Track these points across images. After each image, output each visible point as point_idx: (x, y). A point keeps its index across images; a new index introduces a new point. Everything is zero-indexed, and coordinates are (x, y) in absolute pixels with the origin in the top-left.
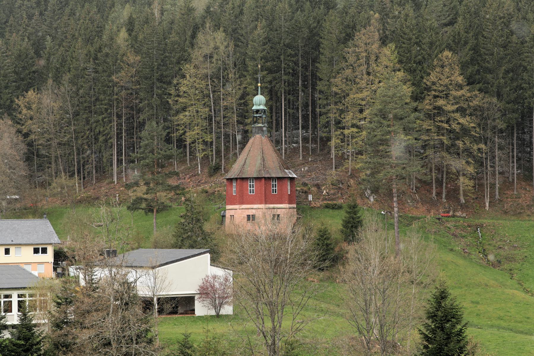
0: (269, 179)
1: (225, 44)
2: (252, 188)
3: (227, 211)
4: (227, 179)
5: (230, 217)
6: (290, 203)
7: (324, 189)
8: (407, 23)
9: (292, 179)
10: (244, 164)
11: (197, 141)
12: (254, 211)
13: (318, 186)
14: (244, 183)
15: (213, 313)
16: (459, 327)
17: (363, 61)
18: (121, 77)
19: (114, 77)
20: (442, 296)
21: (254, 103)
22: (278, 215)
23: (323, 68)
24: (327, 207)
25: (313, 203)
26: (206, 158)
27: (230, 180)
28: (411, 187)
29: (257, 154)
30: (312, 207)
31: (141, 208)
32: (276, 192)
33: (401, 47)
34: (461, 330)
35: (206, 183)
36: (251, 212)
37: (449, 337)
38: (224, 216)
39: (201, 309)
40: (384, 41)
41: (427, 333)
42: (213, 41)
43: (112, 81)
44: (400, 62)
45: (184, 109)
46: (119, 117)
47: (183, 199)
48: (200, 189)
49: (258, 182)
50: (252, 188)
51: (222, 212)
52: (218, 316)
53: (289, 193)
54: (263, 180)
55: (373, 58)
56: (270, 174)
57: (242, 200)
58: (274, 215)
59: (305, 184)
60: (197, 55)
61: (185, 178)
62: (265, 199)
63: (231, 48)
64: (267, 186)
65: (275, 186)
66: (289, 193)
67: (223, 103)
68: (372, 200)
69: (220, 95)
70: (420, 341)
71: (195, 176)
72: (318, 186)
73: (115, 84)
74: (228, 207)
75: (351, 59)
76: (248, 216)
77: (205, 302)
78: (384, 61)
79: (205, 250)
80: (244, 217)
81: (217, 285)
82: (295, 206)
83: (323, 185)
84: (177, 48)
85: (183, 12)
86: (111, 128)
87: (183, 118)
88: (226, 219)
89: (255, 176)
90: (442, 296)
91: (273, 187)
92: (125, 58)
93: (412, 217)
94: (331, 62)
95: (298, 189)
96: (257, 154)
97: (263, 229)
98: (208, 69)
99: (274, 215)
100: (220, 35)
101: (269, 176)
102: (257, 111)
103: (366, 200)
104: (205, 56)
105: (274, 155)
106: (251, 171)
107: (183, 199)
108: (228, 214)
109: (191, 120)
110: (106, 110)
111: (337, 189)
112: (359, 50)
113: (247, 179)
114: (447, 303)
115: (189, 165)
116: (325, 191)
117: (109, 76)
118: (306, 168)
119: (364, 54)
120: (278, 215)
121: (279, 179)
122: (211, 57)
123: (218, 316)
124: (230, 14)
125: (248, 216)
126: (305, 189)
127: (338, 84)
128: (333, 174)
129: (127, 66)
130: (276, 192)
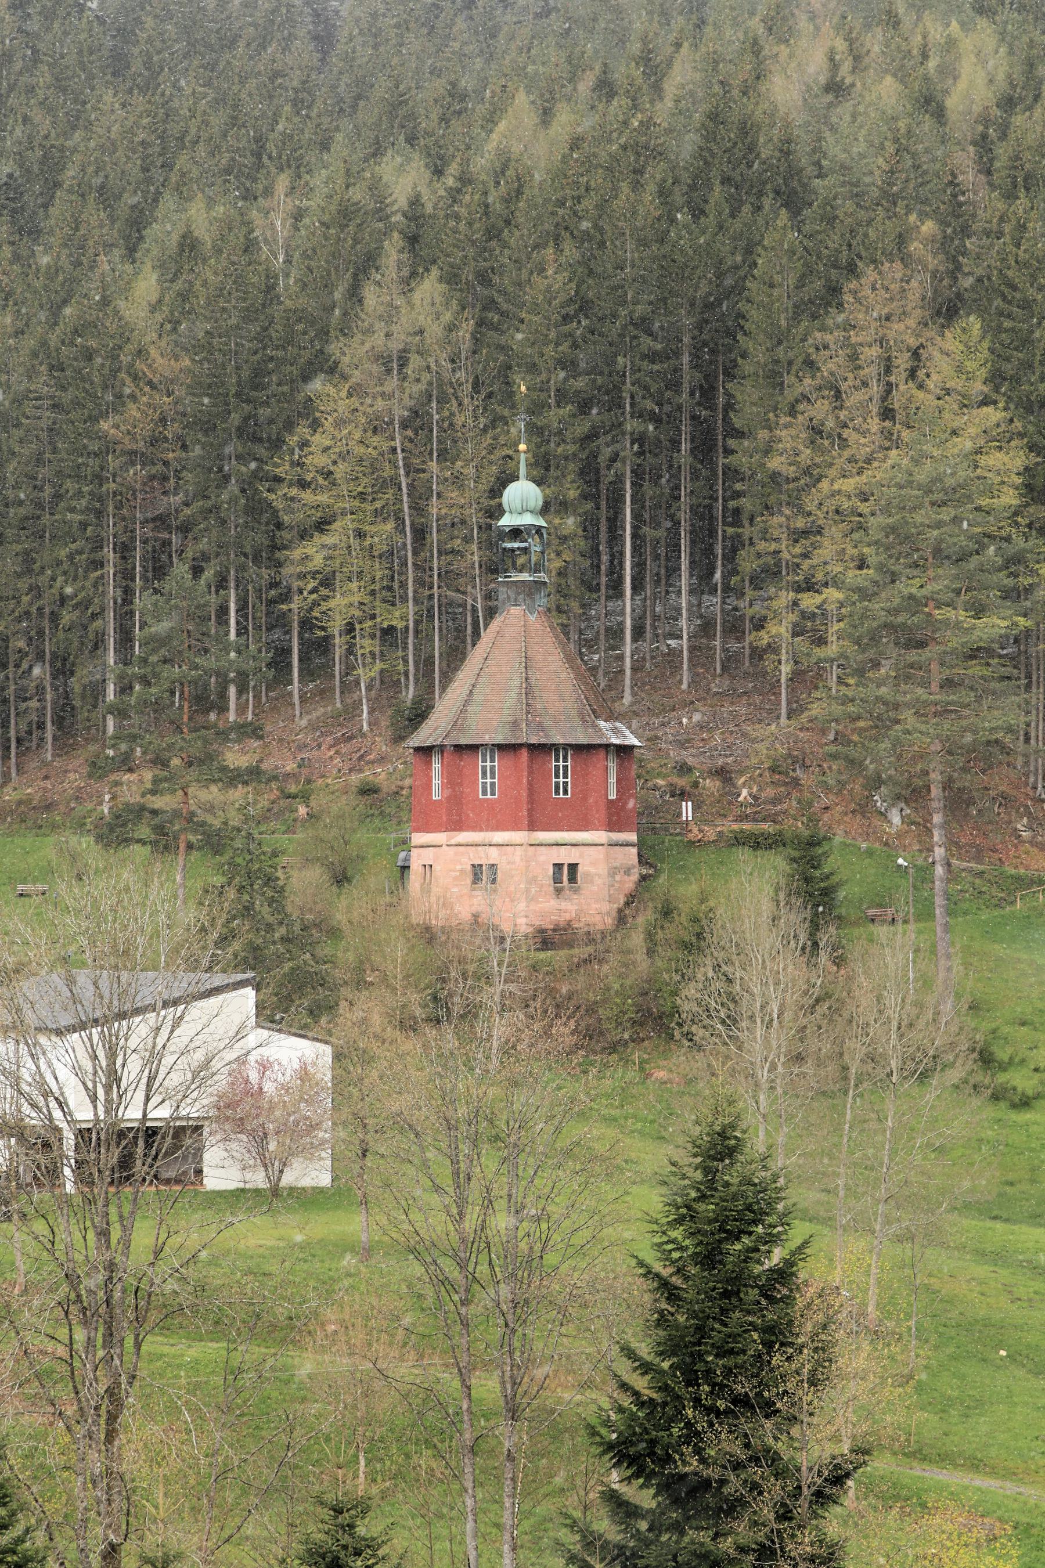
0: (540, 750)
1: (447, 317)
2: (489, 778)
3: (414, 853)
4: (418, 749)
5: (421, 869)
6: (611, 827)
7: (744, 785)
8: (1021, 253)
9: (623, 751)
10: (467, 702)
11: (358, 626)
12: (494, 852)
13: (723, 774)
14: (466, 761)
15: (258, 1179)
16: (777, 1256)
17: (871, 371)
18: (126, 424)
19: (104, 425)
20: (721, 1147)
21: (506, 507)
22: (573, 868)
23: (748, 397)
24: (739, 840)
25: (695, 830)
26: (389, 682)
27: (425, 751)
28: (1032, 779)
29: (513, 669)
30: (691, 843)
31: (139, 841)
32: (566, 792)
33: (1000, 329)
34: (789, 1263)
35: (382, 759)
36: (565, 856)
37: (731, 1292)
38: (405, 868)
39: (222, 1168)
40: (946, 311)
41: (665, 1272)
42: (414, 311)
43: (103, 437)
44: (996, 378)
45: (322, 525)
46: (124, 551)
47: (302, 810)
48: (355, 778)
49: (509, 759)
50: (489, 778)
51: (402, 855)
52: (275, 1191)
53: (613, 796)
54: (525, 753)
55: (903, 361)
56: (547, 736)
57: (456, 816)
58: (558, 867)
59: (684, 769)
60: (353, 353)
61: (319, 746)
62: (531, 812)
63: (465, 332)
64: (541, 772)
65: (561, 773)
66: (613, 796)
67: (435, 508)
68: (896, 820)
69: (429, 481)
70: (647, 1297)
71: (351, 738)
72: (723, 774)
73: (109, 447)
74: (418, 838)
75: (830, 366)
76: (477, 871)
77: (234, 1146)
78: (940, 369)
79: (240, 977)
80: (462, 871)
81: (269, 1087)
82: (633, 837)
83: (741, 773)
84: (305, 333)
85: (326, 218)
86: (95, 585)
87: (313, 553)
88: (412, 877)
89: (499, 740)
90: (721, 1147)
91: (557, 776)
92: (139, 365)
93: (1018, 879)
94: (774, 378)
95: (661, 782)
96: (513, 669)
97: (523, 907)
98: (396, 400)
99: (558, 867)
100: (430, 288)
101: (543, 741)
102: (516, 533)
103: (876, 822)
104: (384, 360)
105: (566, 676)
106: (489, 725)
107: (302, 810)
108: (417, 860)
109: (336, 566)
110: (84, 526)
111: (786, 784)
112: (859, 339)
113: (474, 748)
114: (732, 1175)
115: (338, 705)
116: (745, 792)
117: (94, 419)
118: (697, 717)
119: (874, 351)
120: (573, 868)
121: (579, 748)
122: (403, 362)
123: (275, 1191)
124: (470, 224)
125: (477, 871)
126: (682, 782)
127: (786, 448)
128: (772, 736)
129: (147, 389)
130: (566, 792)
